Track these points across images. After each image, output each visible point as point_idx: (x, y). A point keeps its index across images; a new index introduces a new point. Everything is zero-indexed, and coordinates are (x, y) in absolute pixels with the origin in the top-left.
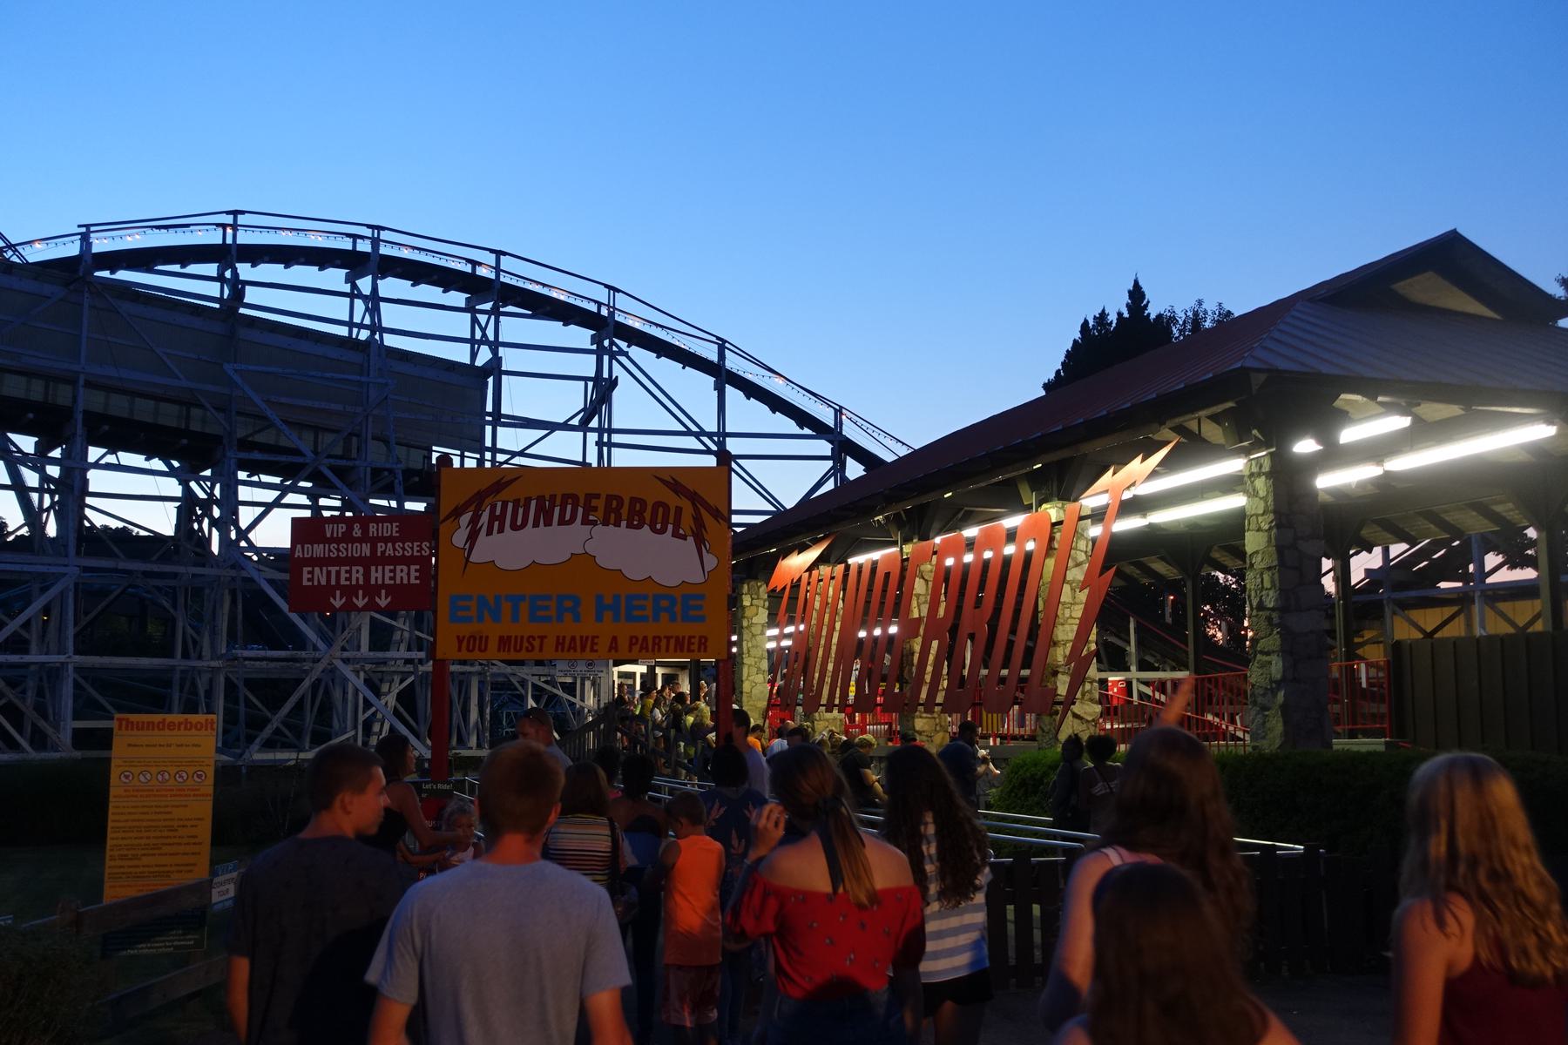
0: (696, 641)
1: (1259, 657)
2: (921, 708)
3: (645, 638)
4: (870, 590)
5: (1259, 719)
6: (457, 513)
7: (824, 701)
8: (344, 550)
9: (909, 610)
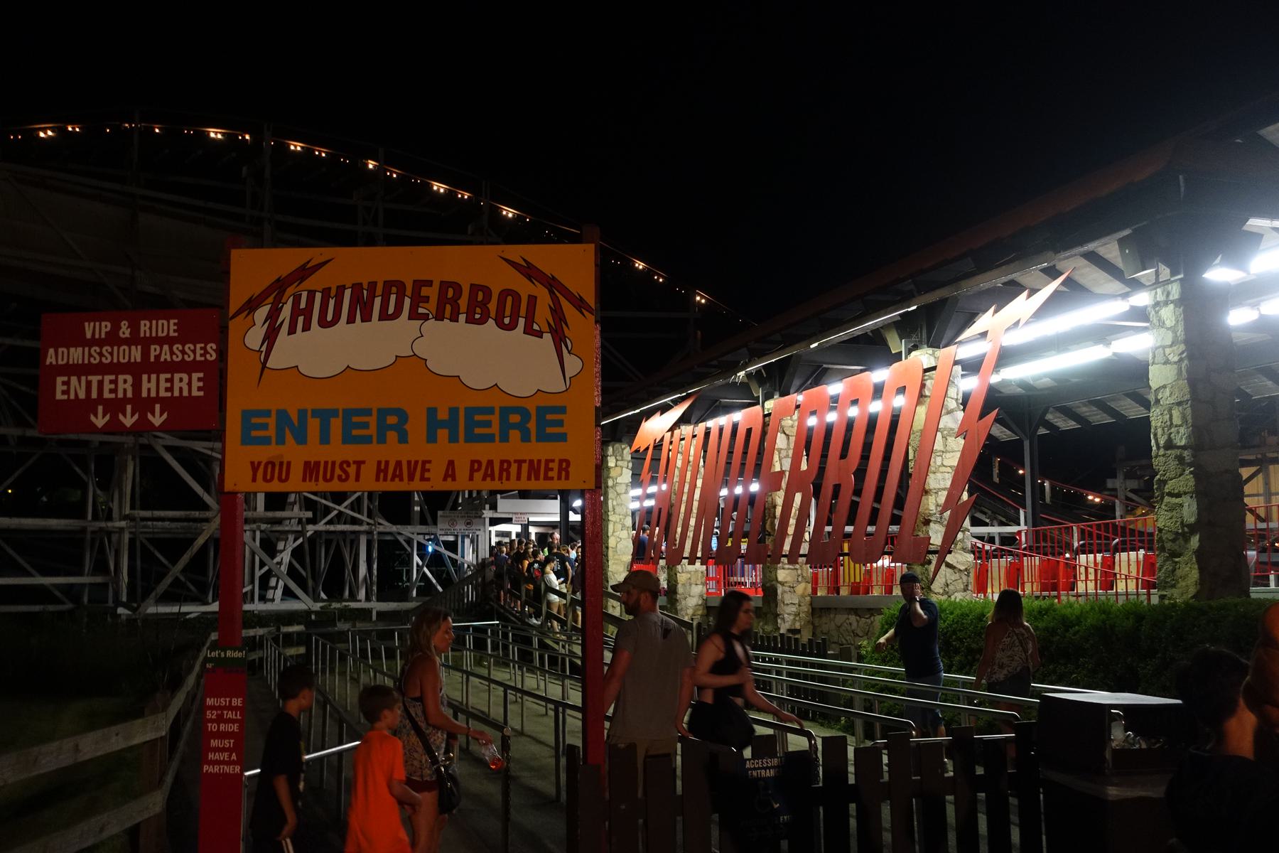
0: (555, 466)
1: (1167, 499)
2: (785, 560)
3: (490, 463)
4: (730, 452)
5: (1168, 566)
6: (251, 306)
7: (686, 554)
8: (109, 355)
9: (771, 464)
